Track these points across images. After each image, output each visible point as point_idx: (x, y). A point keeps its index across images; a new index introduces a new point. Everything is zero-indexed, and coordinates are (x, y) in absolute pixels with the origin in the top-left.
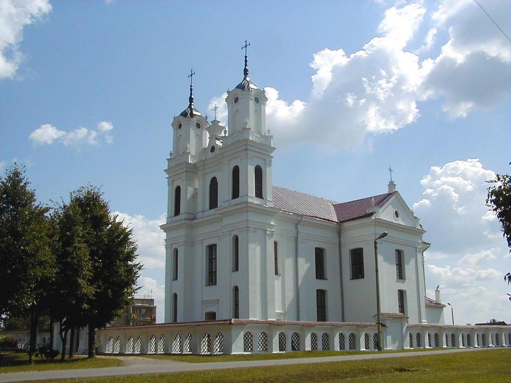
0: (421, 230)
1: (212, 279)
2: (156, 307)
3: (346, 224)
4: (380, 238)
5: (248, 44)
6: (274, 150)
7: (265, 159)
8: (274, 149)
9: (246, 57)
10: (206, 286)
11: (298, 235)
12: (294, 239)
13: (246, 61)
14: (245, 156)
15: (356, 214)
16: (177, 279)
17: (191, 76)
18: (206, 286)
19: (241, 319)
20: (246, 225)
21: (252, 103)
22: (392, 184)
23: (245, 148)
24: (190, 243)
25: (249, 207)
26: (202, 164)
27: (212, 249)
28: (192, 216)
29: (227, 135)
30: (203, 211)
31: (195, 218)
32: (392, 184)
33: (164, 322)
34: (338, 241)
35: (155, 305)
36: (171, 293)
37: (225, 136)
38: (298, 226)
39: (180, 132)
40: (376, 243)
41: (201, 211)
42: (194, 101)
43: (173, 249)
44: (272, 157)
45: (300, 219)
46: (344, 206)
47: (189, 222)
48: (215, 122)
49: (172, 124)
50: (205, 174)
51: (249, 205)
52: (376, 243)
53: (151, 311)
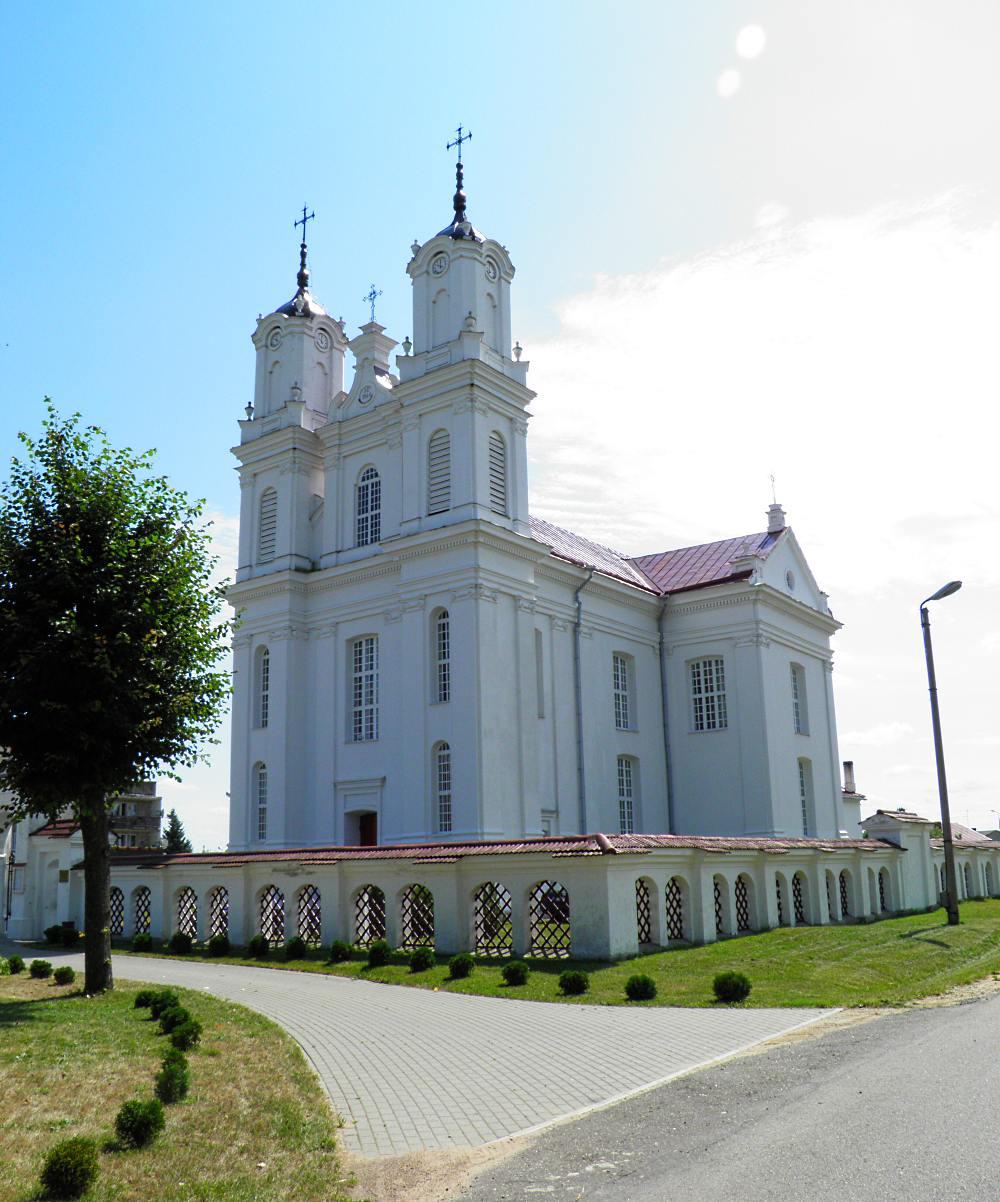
0: (828, 617)
1: (361, 727)
2: (160, 799)
3: (680, 599)
4: (937, 596)
5: (465, 133)
6: (532, 398)
7: (511, 419)
8: (533, 394)
9: (459, 166)
10: (346, 743)
11: (578, 617)
12: (570, 627)
13: (460, 176)
14: (469, 404)
15: (675, 579)
16: (265, 724)
17: (304, 221)
18: (346, 743)
19: (458, 834)
20: (473, 581)
21: (480, 270)
22: (776, 512)
23: (469, 382)
24: (302, 630)
25: (483, 532)
26: (337, 431)
27: (362, 650)
28: (307, 565)
29: (411, 354)
30: (338, 552)
31: (314, 568)
32: (776, 512)
33: (224, 849)
34: (658, 640)
35: (157, 795)
36: (248, 762)
37: (407, 356)
38: (580, 594)
39: (274, 356)
40: (924, 612)
41: (334, 550)
42: (309, 282)
43: (254, 650)
44: (529, 415)
45: (587, 577)
46: (673, 561)
47: (301, 578)
48: (372, 330)
49: (252, 336)
50: (344, 457)
51: (483, 527)
52: (924, 612)
53: (149, 807)
